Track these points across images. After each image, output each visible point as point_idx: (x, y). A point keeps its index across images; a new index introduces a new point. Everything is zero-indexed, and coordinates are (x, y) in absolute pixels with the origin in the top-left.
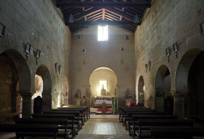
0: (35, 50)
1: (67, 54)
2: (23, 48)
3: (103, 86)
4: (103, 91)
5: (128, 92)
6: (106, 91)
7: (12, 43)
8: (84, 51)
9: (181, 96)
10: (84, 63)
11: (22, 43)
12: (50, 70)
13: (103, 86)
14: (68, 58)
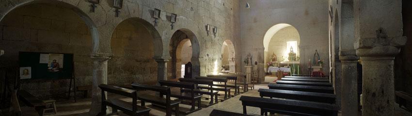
0: (169, 15)
1: (232, 12)
2: (149, 14)
3: (292, 48)
4: (292, 56)
5: (316, 55)
6: (297, 55)
7: (134, 12)
8: (247, 6)
9: (349, 60)
10: (255, 21)
11: (149, 10)
12: (196, 34)
13: (292, 48)
14: (232, 18)
